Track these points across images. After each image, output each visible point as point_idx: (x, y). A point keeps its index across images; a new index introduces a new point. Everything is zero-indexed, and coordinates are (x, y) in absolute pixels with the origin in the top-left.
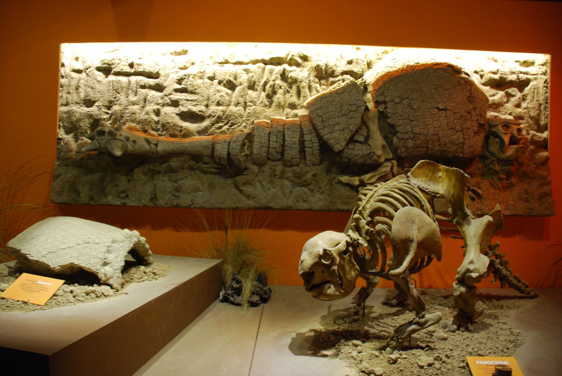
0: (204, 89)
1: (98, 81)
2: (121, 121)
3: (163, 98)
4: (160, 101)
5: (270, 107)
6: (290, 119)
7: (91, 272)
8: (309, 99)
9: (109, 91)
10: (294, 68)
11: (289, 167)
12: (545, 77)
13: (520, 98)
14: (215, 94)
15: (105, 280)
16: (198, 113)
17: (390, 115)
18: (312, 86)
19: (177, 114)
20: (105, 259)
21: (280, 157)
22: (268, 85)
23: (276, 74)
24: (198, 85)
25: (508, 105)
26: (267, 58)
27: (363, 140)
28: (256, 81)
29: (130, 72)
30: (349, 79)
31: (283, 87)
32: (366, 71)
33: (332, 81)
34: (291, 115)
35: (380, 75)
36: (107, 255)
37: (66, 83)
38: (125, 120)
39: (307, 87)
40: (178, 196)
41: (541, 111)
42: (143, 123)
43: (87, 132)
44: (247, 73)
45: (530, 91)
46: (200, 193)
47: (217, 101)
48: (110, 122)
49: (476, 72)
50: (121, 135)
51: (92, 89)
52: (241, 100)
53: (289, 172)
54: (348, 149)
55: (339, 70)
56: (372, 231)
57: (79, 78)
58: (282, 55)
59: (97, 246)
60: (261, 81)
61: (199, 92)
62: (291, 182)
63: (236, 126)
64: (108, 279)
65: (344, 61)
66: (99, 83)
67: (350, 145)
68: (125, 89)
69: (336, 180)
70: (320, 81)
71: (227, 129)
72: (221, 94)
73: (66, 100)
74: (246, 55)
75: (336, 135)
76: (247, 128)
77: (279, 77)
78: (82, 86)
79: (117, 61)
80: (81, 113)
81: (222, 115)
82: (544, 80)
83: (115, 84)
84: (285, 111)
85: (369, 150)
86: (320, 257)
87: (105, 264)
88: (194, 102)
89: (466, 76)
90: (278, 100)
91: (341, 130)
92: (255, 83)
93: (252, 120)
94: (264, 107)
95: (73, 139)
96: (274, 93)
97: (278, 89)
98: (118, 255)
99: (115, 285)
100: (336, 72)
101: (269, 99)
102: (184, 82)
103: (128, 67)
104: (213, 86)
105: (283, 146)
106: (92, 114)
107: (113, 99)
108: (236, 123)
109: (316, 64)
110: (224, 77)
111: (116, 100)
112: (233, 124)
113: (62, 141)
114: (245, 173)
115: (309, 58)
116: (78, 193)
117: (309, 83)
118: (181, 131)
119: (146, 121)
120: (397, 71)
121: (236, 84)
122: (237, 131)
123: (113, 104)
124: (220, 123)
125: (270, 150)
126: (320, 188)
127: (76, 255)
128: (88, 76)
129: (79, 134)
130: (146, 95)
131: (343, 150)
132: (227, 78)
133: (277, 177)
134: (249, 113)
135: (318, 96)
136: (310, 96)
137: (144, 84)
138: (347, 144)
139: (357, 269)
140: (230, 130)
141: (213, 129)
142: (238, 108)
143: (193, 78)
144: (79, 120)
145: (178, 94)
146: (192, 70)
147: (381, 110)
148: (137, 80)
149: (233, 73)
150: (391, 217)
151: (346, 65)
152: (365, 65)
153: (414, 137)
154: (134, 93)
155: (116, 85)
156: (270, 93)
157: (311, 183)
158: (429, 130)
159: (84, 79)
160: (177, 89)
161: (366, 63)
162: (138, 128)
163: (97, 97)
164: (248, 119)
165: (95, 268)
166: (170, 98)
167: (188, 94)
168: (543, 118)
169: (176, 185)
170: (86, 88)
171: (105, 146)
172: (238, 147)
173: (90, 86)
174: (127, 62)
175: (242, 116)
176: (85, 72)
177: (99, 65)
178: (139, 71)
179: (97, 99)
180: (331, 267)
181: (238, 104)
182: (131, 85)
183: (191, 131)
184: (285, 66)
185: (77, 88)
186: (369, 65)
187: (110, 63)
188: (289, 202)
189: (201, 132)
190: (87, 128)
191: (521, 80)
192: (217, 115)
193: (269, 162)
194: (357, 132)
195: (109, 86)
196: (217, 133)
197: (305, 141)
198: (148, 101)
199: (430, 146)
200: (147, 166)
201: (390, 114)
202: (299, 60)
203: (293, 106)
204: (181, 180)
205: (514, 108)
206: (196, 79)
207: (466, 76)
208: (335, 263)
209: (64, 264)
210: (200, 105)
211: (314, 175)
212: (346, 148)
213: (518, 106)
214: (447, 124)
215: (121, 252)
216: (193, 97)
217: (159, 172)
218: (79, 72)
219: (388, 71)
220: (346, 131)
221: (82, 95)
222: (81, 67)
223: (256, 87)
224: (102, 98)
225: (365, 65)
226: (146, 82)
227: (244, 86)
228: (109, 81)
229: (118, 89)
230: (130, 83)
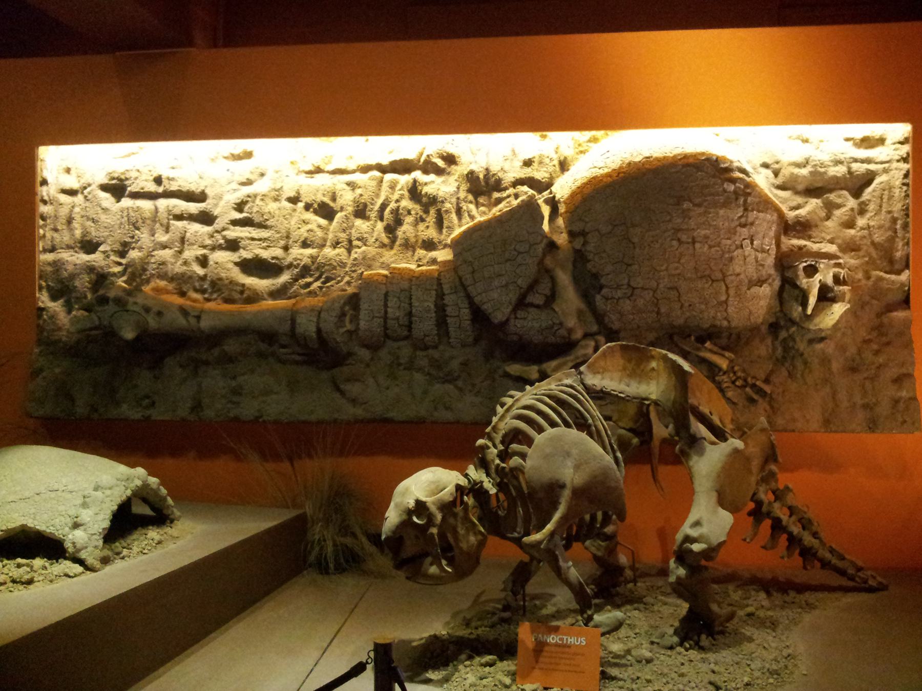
0: (281, 219)
1: (103, 209)
2: (144, 277)
3: (212, 236)
4: (208, 242)
5: (392, 248)
6: (424, 268)
7: (54, 538)
8: (457, 231)
9: (122, 226)
10: (432, 177)
11: (422, 350)
12: (906, 166)
13: (852, 210)
14: (299, 228)
15: (73, 553)
16: (270, 260)
17: (591, 257)
18: (462, 208)
19: (236, 264)
20: (77, 517)
21: (406, 333)
22: (388, 210)
23: (400, 190)
24: (270, 213)
25: (829, 223)
26: (385, 162)
27: (541, 303)
28: (368, 203)
29: (157, 193)
30: (526, 193)
31: (413, 212)
32: (557, 177)
33: (496, 199)
34: (425, 261)
35: (578, 184)
36: (81, 510)
37: (50, 212)
38: (149, 276)
39: (453, 211)
40: (238, 403)
41: (895, 232)
42: (179, 279)
43: (86, 297)
44: (353, 190)
45: (874, 194)
46: (274, 397)
47: (302, 239)
48: (124, 278)
49: (766, 166)
50: (136, 303)
51: (93, 222)
52: (343, 236)
53: (422, 360)
54: (516, 318)
55: (509, 178)
56: (504, 468)
57: (73, 204)
58: (411, 155)
59: (69, 496)
60: (376, 202)
61: (273, 224)
62: (426, 375)
63: (334, 281)
64: (79, 551)
65: (518, 160)
66: (105, 212)
67: (519, 312)
68: (148, 222)
69: (500, 372)
70: (476, 198)
71: (319, 287)
72: (309, 227)
73: (51, 242)
74: (351, 158)
75: (495, 295)
76: (352, 284)
77: (406, 194)
78: (77, 217)
79: (134, 174)
80: (75, 265)
81: (311, 263)
82: (904, 172)
83: (132, 214)
84: (416, 254)
85: (551, 319)
86: (410, 512)
87: (76, 526)
88: (264, 242)
89: (741, 175)
90: (404, 236)
91: (502, 286)
92: (365, 205)
93: (360, 271)
94: (379, 247)
95: (64, 308)
96: (399, 222)
97: (405, 216)
98: (100, 511)
99: (90, 561)
100: (503, 182)
101: (390, 233)
102: (246, 208)
103: (153, 183)
104: (297, 214)
105: (410, 314)
106: (93, 265)
107: (129, 239)
108: (333, 276)
109: (468, 169)
110: (314, 198)
111: (134, 240)
112: (328, 280)
113: (44, 313)
114: (348, 362)
115: (457, 159)
116: (73, 400)
117: (458, 204)
118: (242, 292)
119: (183, 276)
120: (608, 175)
121: (335, 209)
122: (335, 291)
123: (128, 248)
124: (306, 278)
125: (389, 321)
126: (473, 385)
127: (33, 511)
128: (88, 200)
129: (73, 300)
130: (183, 232)
131: (508, 320)
132: (320, 198)
133: (402, 368)
134: (355, 259)
135: (468, 228)
136: (459, 226)
137: (180, 213)
138: (514, 310)
139: (480, 532)
140: (324, 289)
141: (295, 287)
142: (337, 251)
143: (262, 200)
144: (73, 276)
145: (237, 228)
146: (261, 187)
147: (578, 247)
148: (168, 206)
149: (328, 190)
150: (529, 441)
151: (521, 168)
152: (554, 166)
153: (632, 295)
154: (164, 229)
155: (134, 215)
156: (392, 223)
157: (459, 376)
158: (661, 281)
159: (80, 205)
160: (236, 220)
161: (556, 162)
162: (171, 288)
163: (103, 237)
164: (353, 269)
165: (60, 532)
166: (224, 237)
167: (253, 228)
168: (900, 244)
169: (234, 383)
170: (83, 221)
171: (110, 323)
172: (332, 319)
173: (91, 217)
174: (152, 175)
175: (343, 265)
176: (82, 193)
177: (105, 181)
178: (171, 191)
179: (103, 239)
180: (428, 530)
181: (338, 243)
182: (158, 214)
183: (258, 291)
184: (417, 175)
185: (70, 221)
186: (564, 166)
187: (123, 177)
188: (422, 410)
189: (275, 294)
190: (85, 289)
191: (855, 174)
192: (303, 263)
193: (389, 343)
194: (531, 288)
195: (123, 218)
196: (301, 295)
197: (447, 306)
198: (188, 241)
199: (663, 310)
200: (185, 353)
201: (592, 255)
202: (441, 163)
203: (429, 245)
204: (243, 374)
205: (840, 228)
206: (267, 202)
207: (741, 175)
208: (433, 523)
209: (9, 527)
210: (274, 247)
211: (464, 364)
212: (513, 316)
213: (850, 224)
214: (695, 268)
215: (104, 506)
216: (263, 233)
217: (207, 363)
218: (72, 193)
219: (594, 175)
220: (511, 288)
221: (78, 233)
222: (75, 185)
223: (368, 213)
224: (111, 239)
225: (554, 166)
226: (183, 209)
227: (348, 212)
228: (123, 208)
229: (137, 222)
230: (156, 209)
